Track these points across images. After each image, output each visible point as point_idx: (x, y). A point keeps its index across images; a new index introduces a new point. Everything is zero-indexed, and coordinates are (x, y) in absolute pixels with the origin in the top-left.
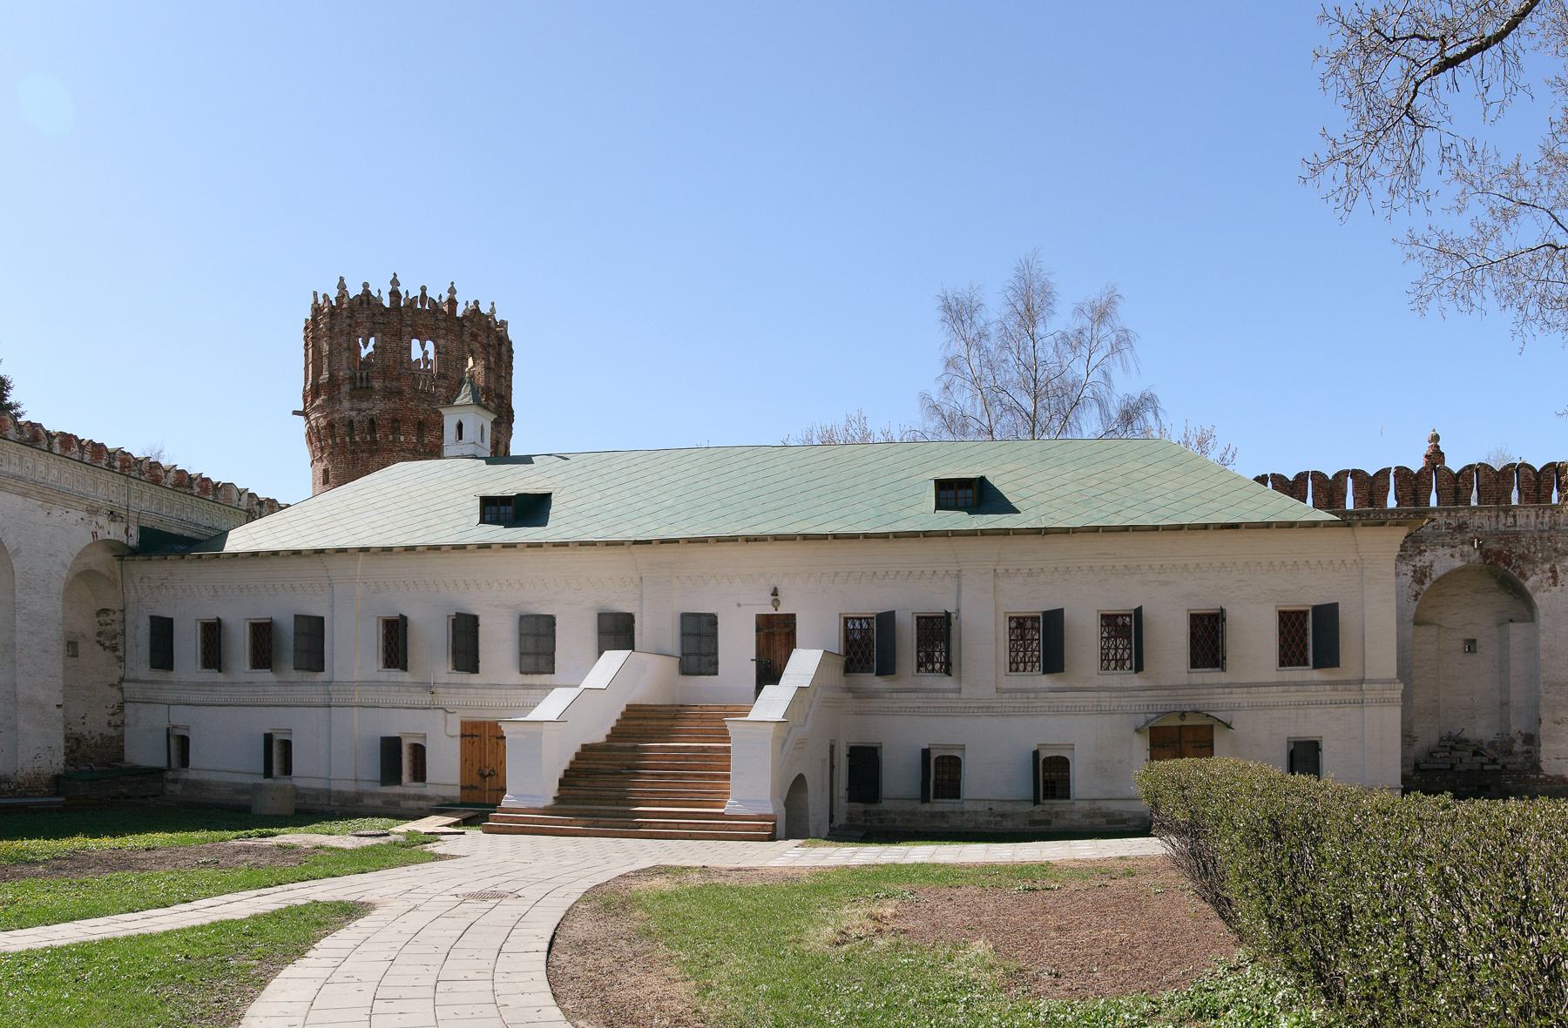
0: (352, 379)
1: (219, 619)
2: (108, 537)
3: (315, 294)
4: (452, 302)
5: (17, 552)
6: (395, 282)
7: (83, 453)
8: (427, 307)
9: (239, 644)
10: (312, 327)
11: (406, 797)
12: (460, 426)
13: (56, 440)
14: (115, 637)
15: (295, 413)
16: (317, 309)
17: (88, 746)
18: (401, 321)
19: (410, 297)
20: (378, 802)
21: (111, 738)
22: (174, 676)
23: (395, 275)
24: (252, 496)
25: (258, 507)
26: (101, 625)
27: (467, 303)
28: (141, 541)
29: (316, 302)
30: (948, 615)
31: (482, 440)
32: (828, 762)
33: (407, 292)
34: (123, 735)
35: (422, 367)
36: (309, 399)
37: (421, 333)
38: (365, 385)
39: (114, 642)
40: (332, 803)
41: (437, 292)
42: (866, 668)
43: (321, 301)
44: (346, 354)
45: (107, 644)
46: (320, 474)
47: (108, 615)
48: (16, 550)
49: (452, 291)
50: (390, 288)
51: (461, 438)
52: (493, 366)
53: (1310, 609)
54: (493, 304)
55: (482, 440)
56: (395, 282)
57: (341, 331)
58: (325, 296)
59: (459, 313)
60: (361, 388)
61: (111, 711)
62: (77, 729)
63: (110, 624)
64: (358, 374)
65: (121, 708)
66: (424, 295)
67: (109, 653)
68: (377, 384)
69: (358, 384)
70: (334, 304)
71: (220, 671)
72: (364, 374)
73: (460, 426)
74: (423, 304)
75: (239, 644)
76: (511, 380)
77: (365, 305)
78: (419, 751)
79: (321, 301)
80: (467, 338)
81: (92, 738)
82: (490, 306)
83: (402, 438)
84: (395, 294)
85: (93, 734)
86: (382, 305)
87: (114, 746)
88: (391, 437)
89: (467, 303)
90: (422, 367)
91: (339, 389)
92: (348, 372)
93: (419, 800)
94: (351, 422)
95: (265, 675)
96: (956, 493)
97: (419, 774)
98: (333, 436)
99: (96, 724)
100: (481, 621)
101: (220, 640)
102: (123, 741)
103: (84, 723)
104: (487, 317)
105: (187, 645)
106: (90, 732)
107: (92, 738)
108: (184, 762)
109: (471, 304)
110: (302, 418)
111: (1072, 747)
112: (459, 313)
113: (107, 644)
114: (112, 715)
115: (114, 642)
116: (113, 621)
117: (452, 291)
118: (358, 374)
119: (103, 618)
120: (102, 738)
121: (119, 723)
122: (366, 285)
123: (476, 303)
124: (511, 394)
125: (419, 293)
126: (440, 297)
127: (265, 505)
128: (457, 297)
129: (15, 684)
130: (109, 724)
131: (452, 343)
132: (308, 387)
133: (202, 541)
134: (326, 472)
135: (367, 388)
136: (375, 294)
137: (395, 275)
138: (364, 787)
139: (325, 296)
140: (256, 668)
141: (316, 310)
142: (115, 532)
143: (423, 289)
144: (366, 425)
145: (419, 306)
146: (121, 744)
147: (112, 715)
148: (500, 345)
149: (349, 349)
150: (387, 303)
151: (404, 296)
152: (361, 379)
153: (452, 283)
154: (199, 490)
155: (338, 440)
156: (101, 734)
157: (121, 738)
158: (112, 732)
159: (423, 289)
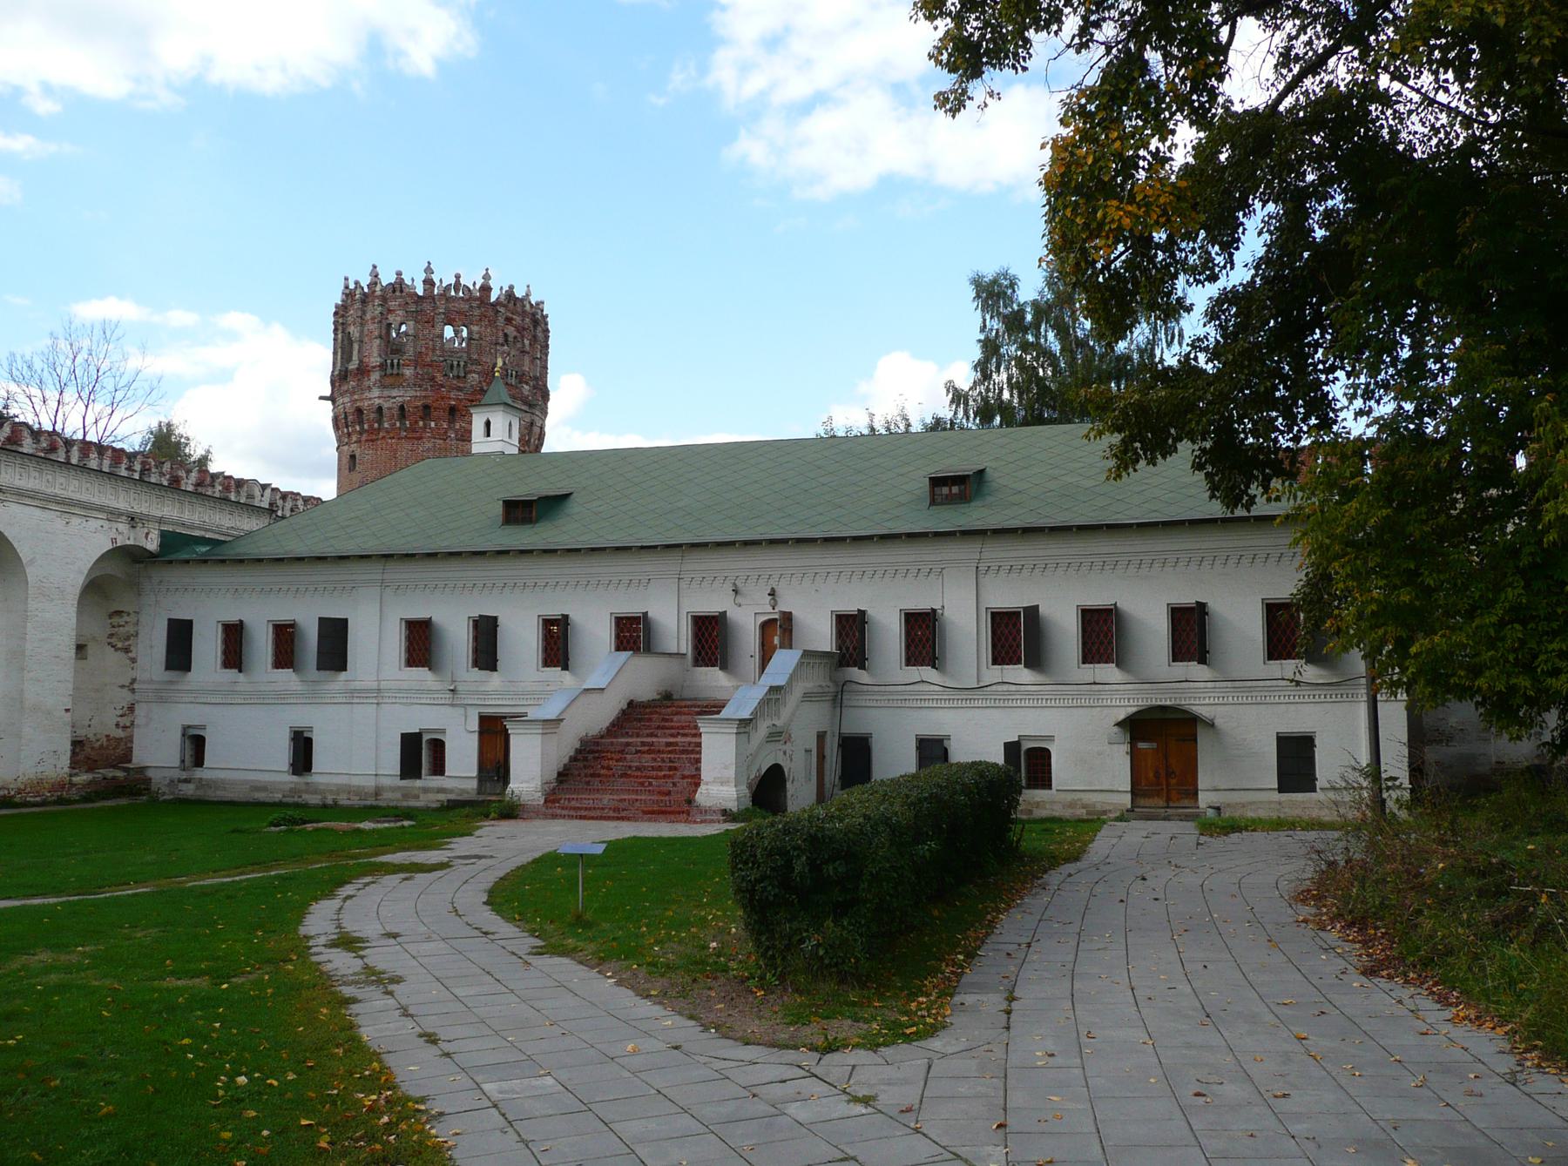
0: (382, 366)
1: (241, 621)
2: (128, 543)
3: (346, 279)
4: (486, 289)
5: (32, 561)
6: (429, 270)
7: (102, 459)
8: (461, 294)
9: (261, 644)
10: (341, 312)
11: (426, 790)
12: (488, 424)
13: (75, 448)
14: (128, 638)
15: (321, 398)
16: (349, 294)
17: (92, 748)
18: (435, 308)
19: (444, 285)
20: (398, 795)
21: (119, 740)
22: (191, 676)
23: (429, 263)
24: (275, 490)
25: (281, 501)
26: (113, 627)
27: (501, 288)
28: (161, 545)
29: (347, 287)
30: (934, 611)
31: (510, 436)
32: (814, 752)
33: (441, 280)
34: (132, 736)
35: (456, 345)
36: (337, 384)
37: (454, 320)
38: (395, 372)
39: (127, 643)
40: (352, 798)
41: (472, 279)
42: (1014, 660)
43: (352, 286)
44: (378, 341)
45: (120, 645)
46: (345, 460)
47: (122, 617)
48: (31, 560)
49: (487, 277)
50: (423, 276)
51: (488, 435)
52: (527, 348)
53: (423, 777)
54: (528, 286)
55: (510, 436)
56: (429, 270)
57: (373, 318)
58: (357, 283)
59: (493, 299)
60: (392, 374)
61: (121, 712)
62: (82, 733)
63: (123, 626)
64: (389, 361)
65: (131, 709)
66: (457, 284)
67: (121, 655)
68: (408, 372)
69: (389, 371)
70: (366, 290)
71: (240, 671)
72: (395, 361)
73: (488, 424)
74: (457, 291)
75: (261, 644)
76: (547, 360)
77: (398, 294)
78: (438, 747)
79: (352, 286)
80: (501, 321)
81: (98, 740)
82: (526, 288)
83: (433, 424)
84: (429, 283)
85: (99, 736)
86: (416, 294)
87: (119, 751)
88: (421, 423)
89: (501, 288)
90: (456, 345)
91: (369, 376)
92: (379, 359)
93: (438, 792)
94: (380, 409)
95: (286, 675)
96: (950, 490)
97: (438, 768)
98: (361, 423)
99: (105, 724)
100: (500, 621)
101: (241, 651)
102: (132, 742)
103: (89, 726)
104: (522, 300)
105: (207, 647)
106: (95, 735)
107: (98, 740)
108: (199, 760)
109: (506, 288)
110: (330, 402)
111: (1051, 738)
112: (493, 299)
113: (120, 645)
114: (121, 716)
115: (127, 643)
116: (126, 622)
117: (487, 277)
118: (389, 361)
119: (116, 620)
120: (108, 740)
121: (128, 724)
122: (399, 274)
123: (511, 287)
124: (547, 373)
125: (453, 281)
126: (475, 283)
127: (289, 499)
128: (491, 283)
129: (22, 690)
130: (117, 725)
131: (486, 328)
132: (336, 373)
133: (224, 542)
134: (353, 457)
135: (398, 374)
136: (408, 282)
137: (429, 263)
138: (386, 782)
139: (357, 283)
140: (277, 668)
141: (347, 295)
142: (127, 536)
143: (458, 277)
144: (396, 412)
145: (453, 293)
146: (129, 745)
147: (121, 716)
148: (535, 327)
149: (380, 337)
150: (420, 292)
151: (438, 284)
152: (392, 365)
153: (487, 270)
154: (220, 488)
155: (366, 426)
156: (107, 736)
157: (130, 739)
158: (120, 733)
159: (458, 277)
